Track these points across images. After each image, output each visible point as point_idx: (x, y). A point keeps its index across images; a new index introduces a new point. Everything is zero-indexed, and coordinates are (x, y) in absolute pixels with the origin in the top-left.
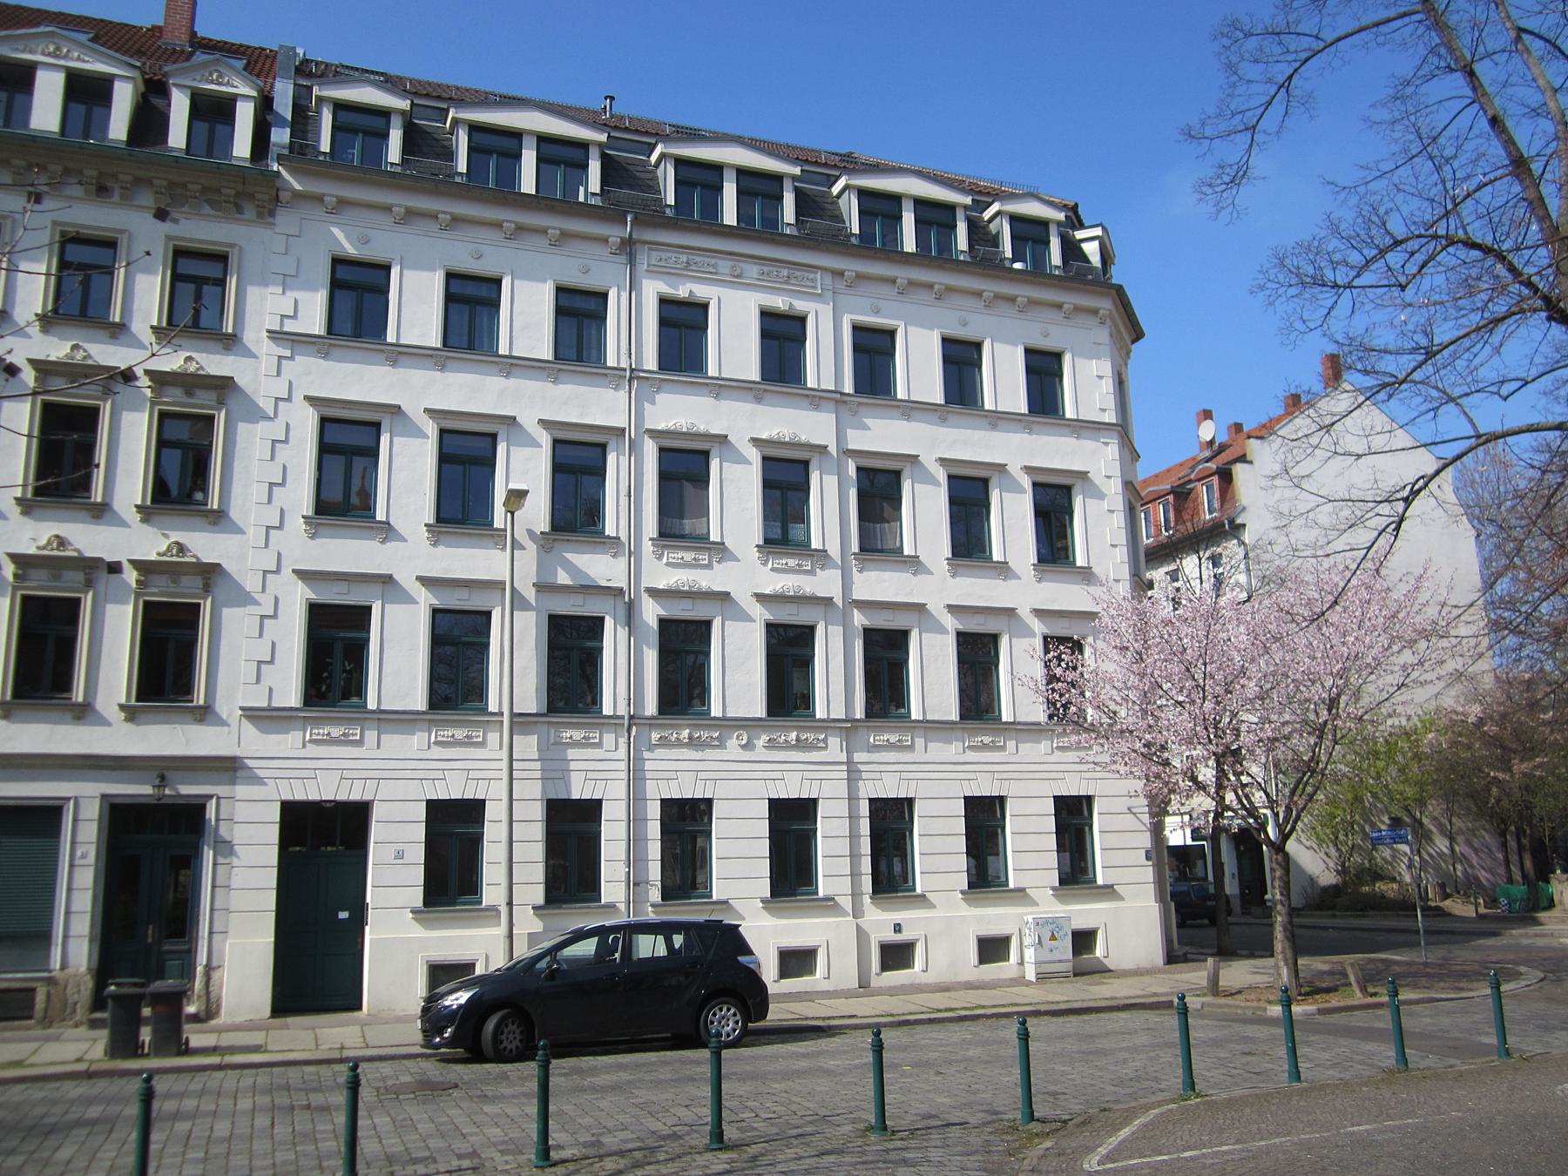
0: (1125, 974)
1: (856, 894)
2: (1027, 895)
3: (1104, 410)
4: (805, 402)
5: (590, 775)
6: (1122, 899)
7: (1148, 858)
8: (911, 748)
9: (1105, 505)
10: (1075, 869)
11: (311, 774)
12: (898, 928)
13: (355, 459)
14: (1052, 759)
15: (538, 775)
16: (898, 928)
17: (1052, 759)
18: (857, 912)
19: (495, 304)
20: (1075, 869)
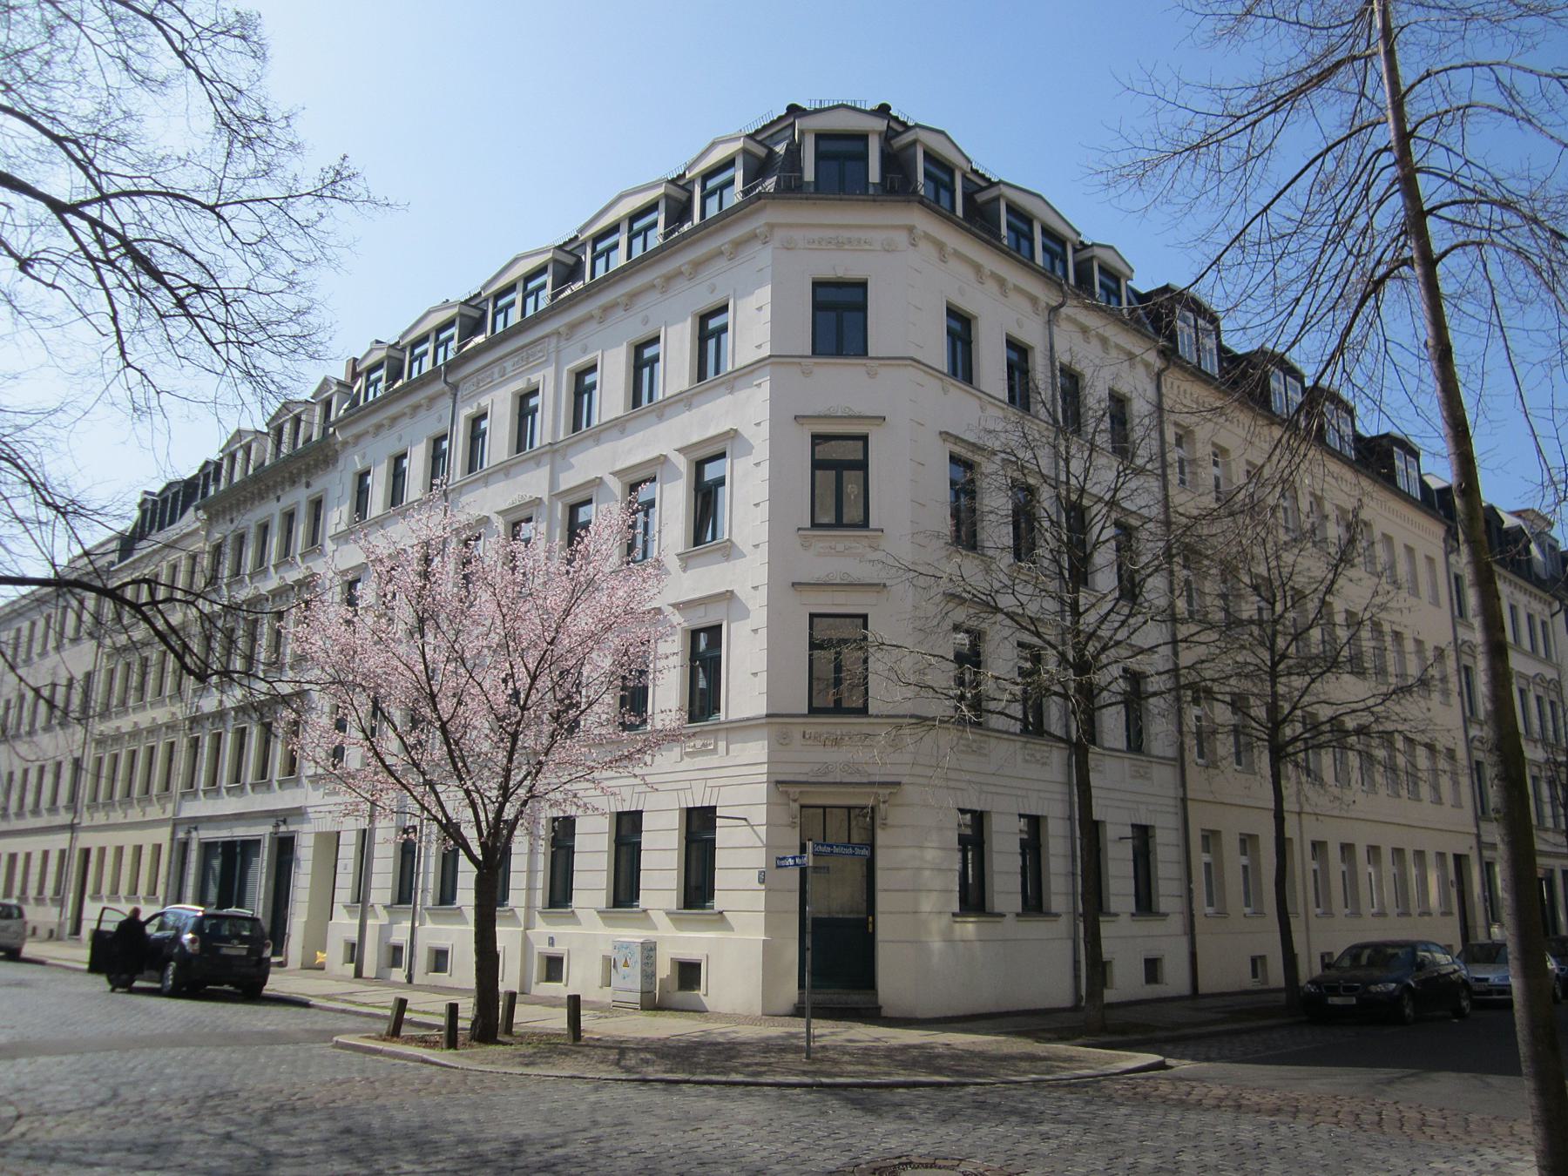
0: (721, 1017)
1: (529, 907)
2: (648, 917)
3: (759, 347)
4: (532, 463)
5: (710, 783)
6: (731, 929)
7: (762, 881)
8: (715, 751)
9: (751, 460)
10: (698, 890)
11: (687, 785)
12: (552, 942)
13: (846, 474)
14: (682, 766)
15: (764, 778)
16: (552, 942)
17: (682, 766)
18: (528, 926)
19: (862, 308)
20: (698, 890)
